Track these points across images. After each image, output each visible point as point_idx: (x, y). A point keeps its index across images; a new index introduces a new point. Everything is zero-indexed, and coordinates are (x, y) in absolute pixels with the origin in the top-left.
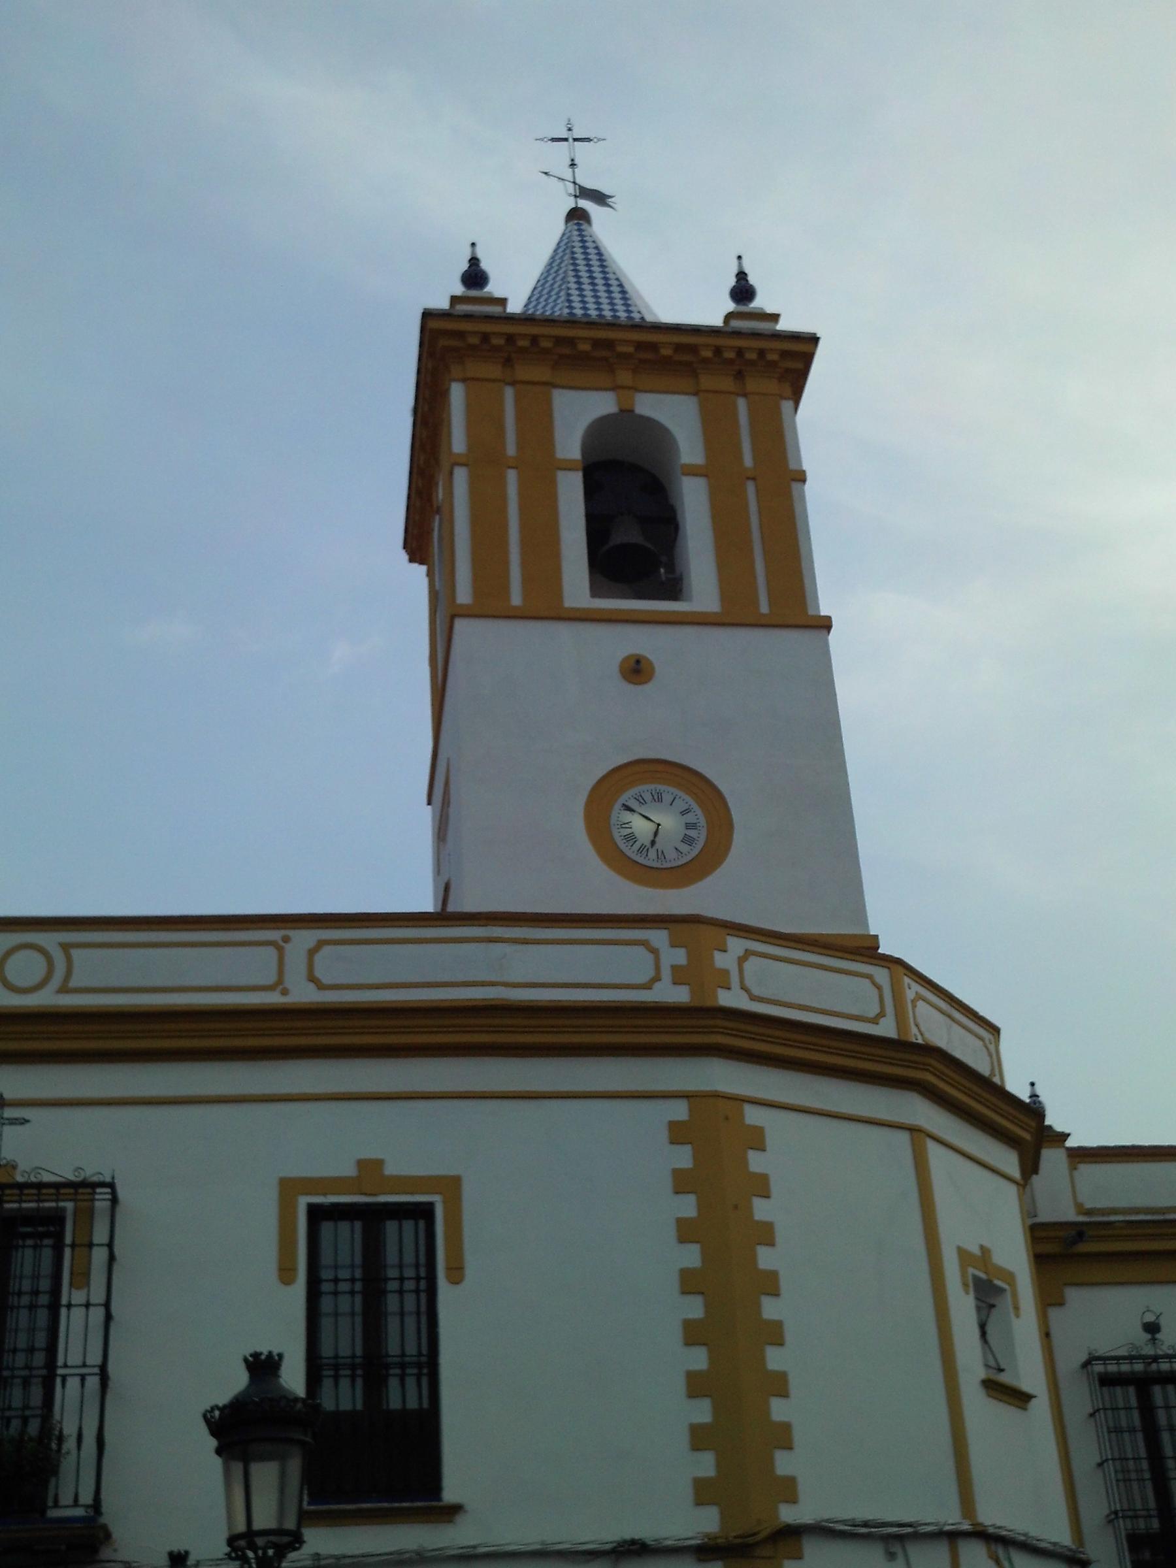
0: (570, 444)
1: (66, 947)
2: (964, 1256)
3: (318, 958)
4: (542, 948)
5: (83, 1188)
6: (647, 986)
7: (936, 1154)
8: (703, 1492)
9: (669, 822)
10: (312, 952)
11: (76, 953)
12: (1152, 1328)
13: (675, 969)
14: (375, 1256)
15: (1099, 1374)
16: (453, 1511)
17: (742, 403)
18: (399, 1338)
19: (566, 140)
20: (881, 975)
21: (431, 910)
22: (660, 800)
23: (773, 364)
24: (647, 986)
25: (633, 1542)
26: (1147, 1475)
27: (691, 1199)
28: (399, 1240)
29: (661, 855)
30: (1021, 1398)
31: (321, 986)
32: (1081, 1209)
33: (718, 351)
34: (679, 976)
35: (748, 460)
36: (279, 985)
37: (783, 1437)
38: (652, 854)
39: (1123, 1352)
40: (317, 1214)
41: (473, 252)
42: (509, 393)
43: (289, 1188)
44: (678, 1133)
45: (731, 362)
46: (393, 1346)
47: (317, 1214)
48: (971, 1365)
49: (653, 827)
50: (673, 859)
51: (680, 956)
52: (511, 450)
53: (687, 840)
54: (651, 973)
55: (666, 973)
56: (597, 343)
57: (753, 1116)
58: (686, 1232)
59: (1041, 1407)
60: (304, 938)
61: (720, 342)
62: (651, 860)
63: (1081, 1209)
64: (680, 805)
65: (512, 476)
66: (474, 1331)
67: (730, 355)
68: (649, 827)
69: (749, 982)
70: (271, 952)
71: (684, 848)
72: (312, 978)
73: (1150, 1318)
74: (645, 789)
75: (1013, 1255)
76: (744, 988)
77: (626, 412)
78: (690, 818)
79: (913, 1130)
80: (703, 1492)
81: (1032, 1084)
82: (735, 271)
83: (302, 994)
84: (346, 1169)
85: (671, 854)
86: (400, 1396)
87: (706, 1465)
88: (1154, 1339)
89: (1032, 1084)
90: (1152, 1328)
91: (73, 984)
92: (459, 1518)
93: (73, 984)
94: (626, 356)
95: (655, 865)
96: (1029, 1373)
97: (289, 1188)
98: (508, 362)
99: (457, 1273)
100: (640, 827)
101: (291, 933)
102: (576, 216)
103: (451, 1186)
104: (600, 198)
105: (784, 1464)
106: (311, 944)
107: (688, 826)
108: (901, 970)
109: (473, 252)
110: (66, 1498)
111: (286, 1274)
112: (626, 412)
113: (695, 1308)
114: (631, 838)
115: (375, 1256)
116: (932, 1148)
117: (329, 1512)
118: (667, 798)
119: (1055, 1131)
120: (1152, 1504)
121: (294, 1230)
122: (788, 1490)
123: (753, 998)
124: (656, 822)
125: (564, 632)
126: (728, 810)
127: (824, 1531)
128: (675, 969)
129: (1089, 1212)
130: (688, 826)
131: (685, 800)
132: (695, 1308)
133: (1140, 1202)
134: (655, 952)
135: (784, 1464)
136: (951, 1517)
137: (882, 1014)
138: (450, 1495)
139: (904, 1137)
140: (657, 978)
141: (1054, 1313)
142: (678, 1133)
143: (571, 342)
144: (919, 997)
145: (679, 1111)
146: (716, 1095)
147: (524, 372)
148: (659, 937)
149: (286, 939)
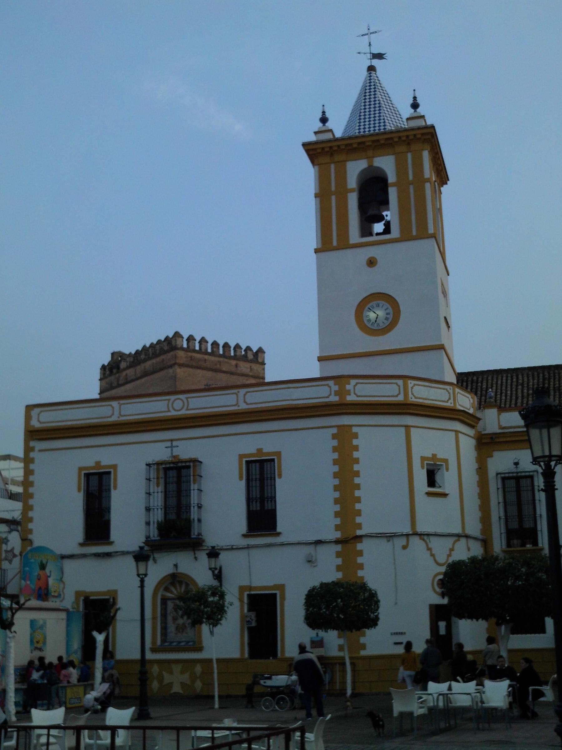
0: (352, 182)
1: (187, 398)
2: (423, 459)
3: (246, 396)
4: (300, 389)
6: (328, 397)
8: (337, 528)
9: (381, 313)
10: (245, 395)
11: (189, 400)
12: (516, 464)
13: (335, 391)
14: (260, 475)
16: (279, 534)
17: (409, 155)
19: (367, 34)
22: (379, 306)
23: (420, 139)
24: (328, 397)
25: (319, 540)
27: (337, 454)
29: (378, 325)
31: (247, 404)
32: (501, 428)
33: (400, 138)
34: (336, 393)
35: (411, 177)
36: (237, 404)
37: (359, 513)
38: (376, 325)
40: (248, 463)
41: (323, 109)
42: (333, 166)
43: (241, 457)
44: (334, 437)
45: (405, 141)
47: (248, 463)
49: (376, 315)
50: (382, 326)
51: (336, 388)
52: (333, 189)
53: (387, 319)
54: (329, 394)
55: (333, 393)
56: (359, 144)
57: (355, 430)
58: (335, 462)
61: (401, 134)
62: (375, 327)
64: (385, 307)
65: (333, 198)
66: (285, 492)
67: (404, 138)
68: (375, 315)
69: (356, 392)
70: (235, 396)
71: (385, 322)
72: (245, 402)
73: (516, 461)
74: (374, 303)
76: (355, 394)
77: (371, 167)
78: (388, 311)
80: (337, 528)
82: (412, 96)
83: (243, 406)
84: (254, 451)
85: (381, 324)
86: (268, 506)
87: (338, 521)
88: (517, 467)
90: (516, 464)
91: (189, 408)
92: (281, 536)
93: (189, 408)
94: (369, 146)
95: (377, 328)
97: (241, 457)
98: (332, 155)
99: (280, 476)
100: (372, 315)
101: (240, 390)
102: (371, 69)
103: (279, 454)
104: (379, 56)
105: (358, 520)
106: (244, 392)
107: (388, 314)
109: (323, 109)
110: (194, 534)
111: (241, 478)
112: (371, 167)
113: (337, 482)
114: (369, 320)
116: (460, 435)
117: (270, 534)
118: (381, 305)
121: (242, 468)
122: (359, 526)
123: (358, 396)
124: (377, 314)
125: (349, 253)
126: (399, 306)
127: (366, 536)
128: (335, 391)
130: (388, 314)
131: (387, 305)
132: (337, 482)
134: (330, 387)
135: (358, 520)
136: (408, 530)
137: (450, 399)
138: (279, 530)
139: (454, 433)
140: (330, 395)
142: (334, 437)
143: (350, 145)
144: (458, 393)
145: (335, 430)
146: (344, 426)
147: (337, 158)
148: (331, 383)
149: (238, 392)
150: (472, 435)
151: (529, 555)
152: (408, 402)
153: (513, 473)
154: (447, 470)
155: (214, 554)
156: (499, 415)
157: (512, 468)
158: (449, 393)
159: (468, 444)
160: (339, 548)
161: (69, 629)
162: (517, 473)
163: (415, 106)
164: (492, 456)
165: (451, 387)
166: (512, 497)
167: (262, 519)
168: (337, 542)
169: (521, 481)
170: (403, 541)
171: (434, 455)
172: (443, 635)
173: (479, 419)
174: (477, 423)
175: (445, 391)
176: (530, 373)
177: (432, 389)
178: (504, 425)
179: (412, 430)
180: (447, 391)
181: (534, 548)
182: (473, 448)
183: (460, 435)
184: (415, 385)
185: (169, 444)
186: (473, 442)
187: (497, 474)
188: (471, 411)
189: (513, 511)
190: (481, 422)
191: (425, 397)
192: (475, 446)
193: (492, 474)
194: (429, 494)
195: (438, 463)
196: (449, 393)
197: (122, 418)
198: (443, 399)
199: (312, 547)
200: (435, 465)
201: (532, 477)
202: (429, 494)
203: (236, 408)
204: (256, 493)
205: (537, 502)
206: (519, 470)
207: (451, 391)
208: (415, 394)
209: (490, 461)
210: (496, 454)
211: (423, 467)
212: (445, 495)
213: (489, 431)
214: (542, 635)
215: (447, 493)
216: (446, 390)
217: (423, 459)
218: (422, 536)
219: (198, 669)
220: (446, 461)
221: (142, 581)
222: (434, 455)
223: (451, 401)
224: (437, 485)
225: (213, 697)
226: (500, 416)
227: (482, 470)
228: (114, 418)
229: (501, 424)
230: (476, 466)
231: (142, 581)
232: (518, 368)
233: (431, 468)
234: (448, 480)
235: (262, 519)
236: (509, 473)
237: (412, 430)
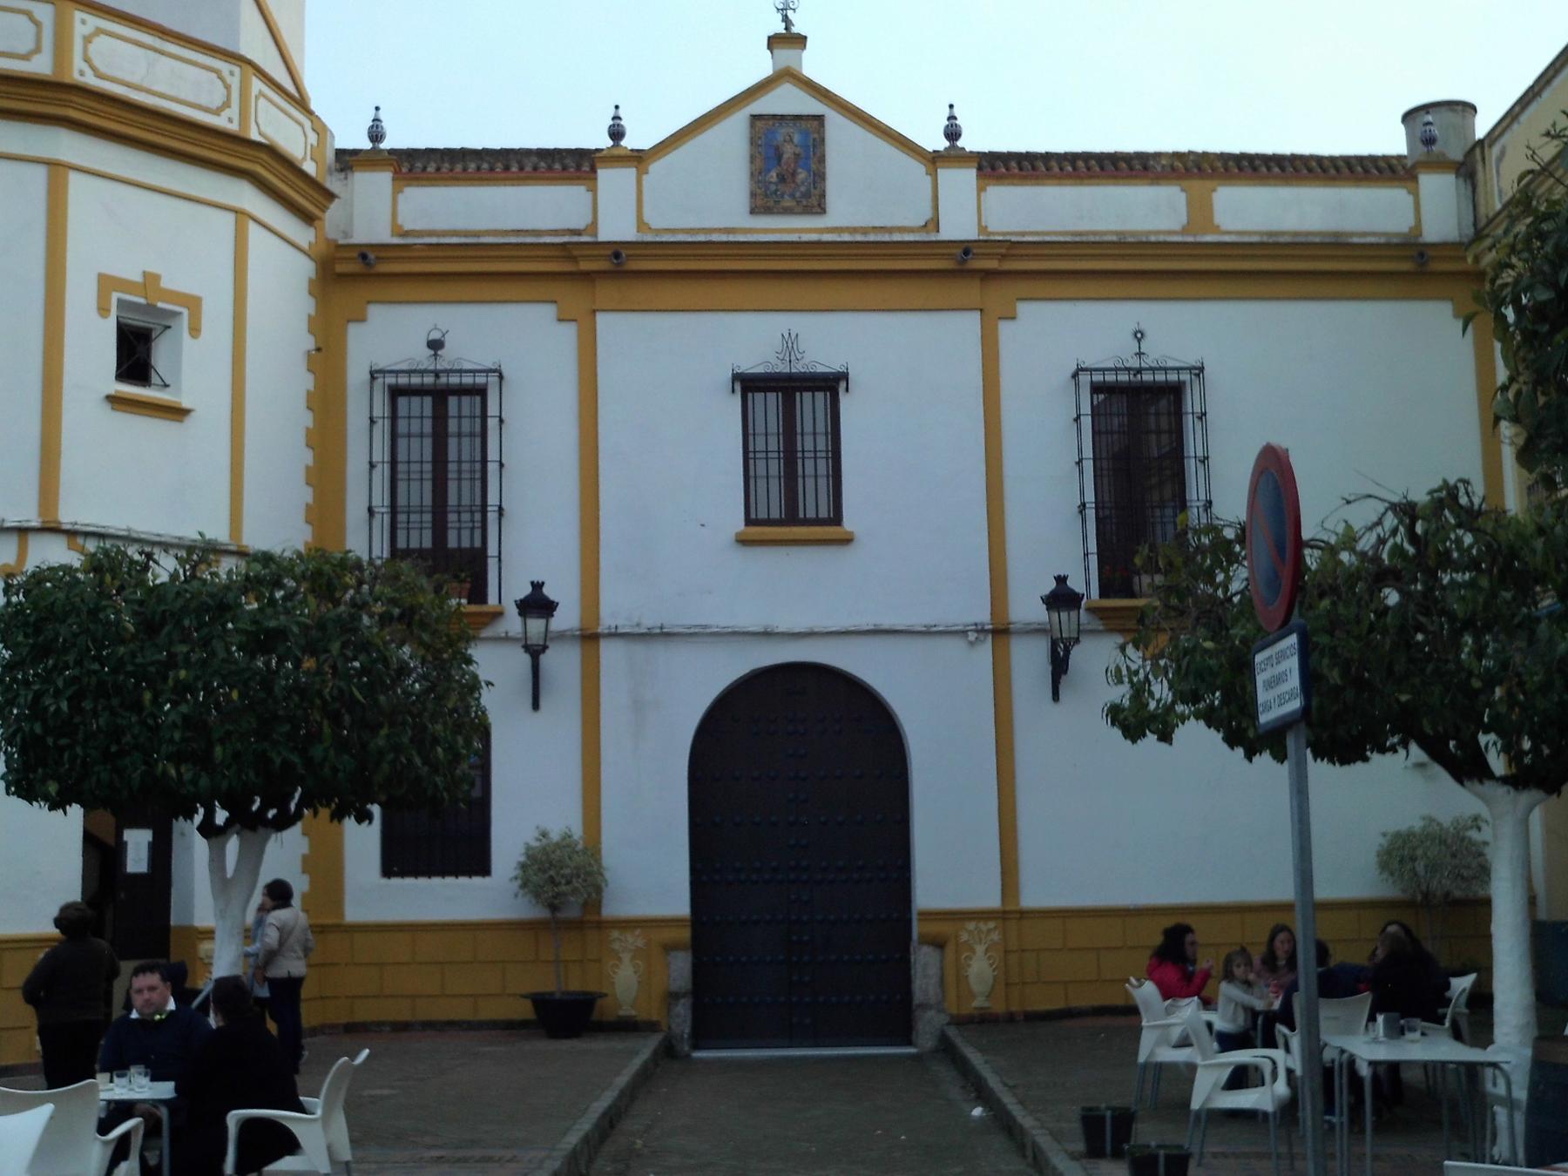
2: (106, 283)
6: (25, 58)
7: (254, 232)
12: (435, 345)
15: (390, 386)
26: (428, 476)
32: (398, 231)
39: (404, 367)
63: (398, 231)
73: (435, 335)
79: (239, 213)
81: (377, 109)
88: (436, 355)
89: (377, 109)
90: (435, 345)
108: (250, 70)
116: (253, 228)
120: (428, 501)
129: (406, 234)
133: (461, 225)
137: (227, 104)
139: (230, 218)
144: (261, 94)
150: (305, 246)
151: (1404, 698)
152: (67, 80)
153: (422, 372)
154: (195, 331)
156: (396, 191)
157: (422, 356)
158: (228, 87)
159: (280, 268)
161: (972, 636)
162: (437, 374)
164: (362, 319)
165: (237, 70)
166: (419, 450)
169: (452, 401)
171: (151, 279)
172: (137, 877)
173: (330, 196)
174: (324, 209)
175: (214, 75)
176: (543, 164)
177: (164, 59)
178: (408, 226)
179: (75, 181)
180: (221, 78)
181: (474, 608)
182: (303, 286)
183: (253, 228)
184: (99, 31)
186: (305, 268)
187: (373, 375)
188: (309, 167)
189: (418, 493)
190: (334, 206)
191: (135, 79)
192: (311, 281)
193: (356, 375)
194: (115, 401)
195: (160, 305)
196: (228, 87)
198: (204, 102)
200: (150, 309)
202: (115, 401)
205: (492, 468)
206: (442, 365)
207: (235, 82)
208: (97, 63)
210: (378, 314)
211: (103, 310)
212: (177, 413)
213: (361, 237)
214: (477, 880)
215: (185, 404)
216: (218, 73)
217: (106, 283)
218: (80, 540)
220: (194, 304)
222: (151, 279)
223: (233, 111)
224: (155, 379)
226: (401, 197)
227: (326, 357)
229: (400, 221)
230: (309, 343)
232: (512, 150)
233: (137, 320)
234: (192, 366)
236: (410, 372)
237: (74, 177)
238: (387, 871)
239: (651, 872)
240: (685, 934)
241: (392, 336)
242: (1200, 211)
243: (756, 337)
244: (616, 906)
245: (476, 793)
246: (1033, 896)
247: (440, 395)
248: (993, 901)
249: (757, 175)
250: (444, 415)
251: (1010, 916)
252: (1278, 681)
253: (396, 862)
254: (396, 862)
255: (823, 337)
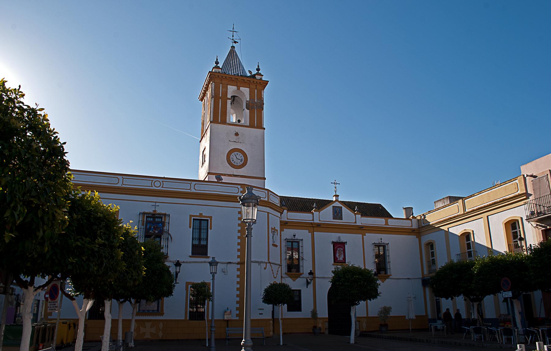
5: (165, 215)
14: (201, 225)
18: (203, 236)
20: (266, 192)
21: (495, 317)
28: (204, 224)
30: (276, 246)
46: (202, 237)
48: (271, 243)
51: (242, 189)
59: (279, 247)
60: (194, 183)
75: (278, 228)
90: (294, 236)
96: (278, 243)
99: (211, 229)
115: (201, 225)
119: (290, 289)
136: (267, 261)
141: (282, 232)
148: (239, 187)
155: (213, 263)
160: (239, 266)
163: (258, 70)
167: (200, 249)
168: (238, 264)
170: (264, 265)
185: (154, 204)
197: (123, 186)
199: (225, 265)
201: (298, 242)
203: (190, 191)
204: (197, 236)
209: (422, 238)
219: (161, 325)
221: (213, 276)
225: (206, 340)
228: (119, 185)
231: (213, 276)
235: (200, 249)
238: (288, 311)
239: (323, 312)
240: (327, 320)
241: (288, 233)
242: (387, 223)
243: (335, 236)
244: (319, 316)
245: (296, 299)
246: (369, 316)
247: (200, 220)
248: (366, 316)
249: (334, 214)
250: (294, 245)
251: (367, 318)
252: (103, 224)
253: (289, 310)
254: (289, 310)
255: (344, 237)
